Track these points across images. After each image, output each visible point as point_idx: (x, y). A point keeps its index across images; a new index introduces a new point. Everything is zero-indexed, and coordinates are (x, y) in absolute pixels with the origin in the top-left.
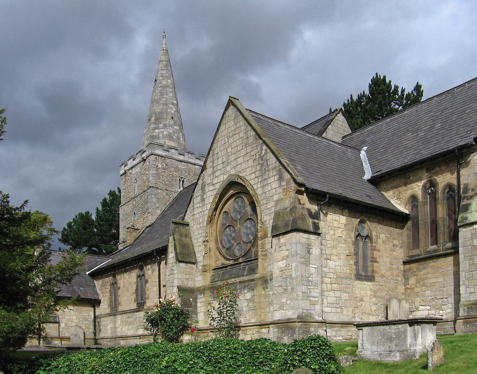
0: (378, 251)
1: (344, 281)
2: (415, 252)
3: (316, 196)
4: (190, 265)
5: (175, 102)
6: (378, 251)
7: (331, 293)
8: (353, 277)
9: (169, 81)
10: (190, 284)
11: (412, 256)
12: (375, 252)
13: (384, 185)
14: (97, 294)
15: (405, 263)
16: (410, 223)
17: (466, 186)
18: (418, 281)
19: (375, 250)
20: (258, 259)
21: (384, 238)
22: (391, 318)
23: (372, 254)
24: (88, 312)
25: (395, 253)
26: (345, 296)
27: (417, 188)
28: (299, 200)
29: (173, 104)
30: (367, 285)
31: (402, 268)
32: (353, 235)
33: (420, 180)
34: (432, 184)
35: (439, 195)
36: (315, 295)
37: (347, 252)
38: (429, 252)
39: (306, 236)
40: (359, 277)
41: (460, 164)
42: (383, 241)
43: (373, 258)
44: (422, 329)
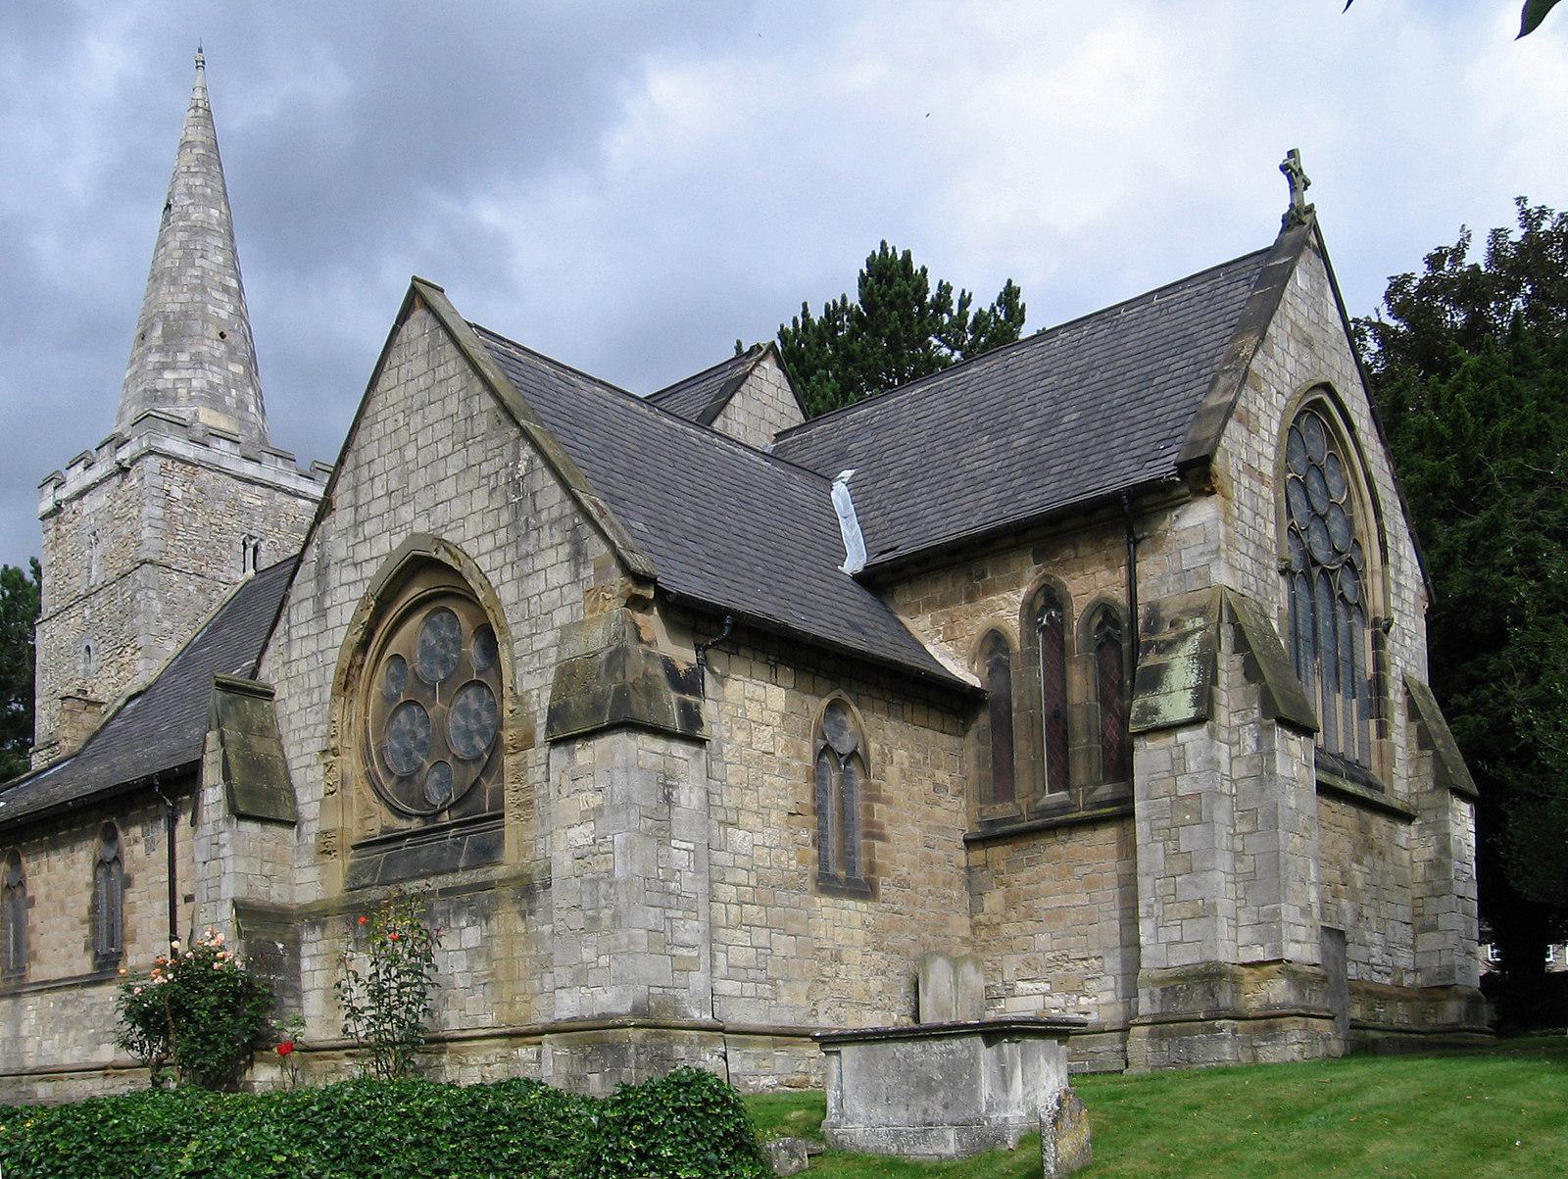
0: (888, 801)
1: (782, 895)
2: (1002, 810)
5: (234, 284)
6: (888, 801)
7: (738, 934)
8: (810, 885)
9: (214, 212)
10: (277, 895)
12: (877, 806)
18: (1010, 903)
19: (878, 799)
21: (906, 765)
23: (869, 811)
27: (1006, 607)
28: (637, 629)
30: (854, 910)
31: (961, 857)
32: (808, 749)
33: (1015, 583)
34: (1051, 598)
36: (688, 938)
39: (659, 745)
40: (827, 884)
41: (1137, 543)
43: (870, 823)
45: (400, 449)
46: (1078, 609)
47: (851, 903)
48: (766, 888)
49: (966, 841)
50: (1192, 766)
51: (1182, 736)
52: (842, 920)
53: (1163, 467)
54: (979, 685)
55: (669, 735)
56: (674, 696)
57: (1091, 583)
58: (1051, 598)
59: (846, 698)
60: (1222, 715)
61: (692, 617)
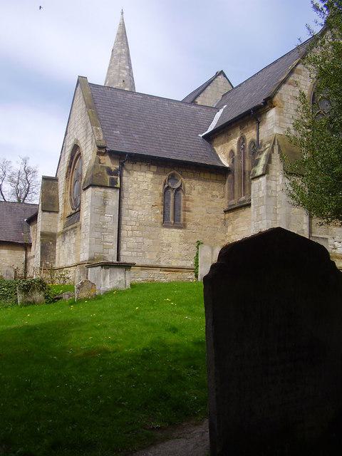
0: (192, 201)
1: (148, 228)
2: (233, 202)
3: (115, 155)
4: (53, 214)
5: (128, 67)
6: (192, 201)
7: (131, 239)
8: (159, 225)
9: (124, 50)
10: (52, 230)
11: (230, 206)
12: (187, 203)
13: (216, 142)
14: (30, 238)
15: (226, 212)
16: (230, 176)
17: (262, 141)
18: (233, 230)
19: (188, 200)
20: (249, 205)
21: (200, 190)
22: (123, 260)
23: (185, 204)
24: (20, 255)
25: (214, 204)
26: (148, 242)
27: (234, 144)
28: (100, 160)
29: (125, 69)
30: (175, 233)
31: (223, 216)
32: (161, 188)
33: (235, 137)
34: (243, 139)
35: (247, 150)
36: (109, 240)
37: (153, 203)
38: (240, 202)
39: (103, 190)
40: (165, 223)
41: (259, 123)
42: (199, 193)
43: (185, 207)
44: (110, 272)
45: (194, 102)
46: (248, 141)
47: (176, 230)
48: (142, 225)
49: (225, 212)
50: (263, 188)
51: (261, 179)
52: (171, 235)
53: (260, 102)
54: (227, 165)
55: (106, 187)
56: (109, 177)
57: (251, 135)
58: (243, 139)
59: (176, 173)
60: (273, 172)
61: (115, 155)
